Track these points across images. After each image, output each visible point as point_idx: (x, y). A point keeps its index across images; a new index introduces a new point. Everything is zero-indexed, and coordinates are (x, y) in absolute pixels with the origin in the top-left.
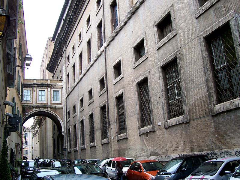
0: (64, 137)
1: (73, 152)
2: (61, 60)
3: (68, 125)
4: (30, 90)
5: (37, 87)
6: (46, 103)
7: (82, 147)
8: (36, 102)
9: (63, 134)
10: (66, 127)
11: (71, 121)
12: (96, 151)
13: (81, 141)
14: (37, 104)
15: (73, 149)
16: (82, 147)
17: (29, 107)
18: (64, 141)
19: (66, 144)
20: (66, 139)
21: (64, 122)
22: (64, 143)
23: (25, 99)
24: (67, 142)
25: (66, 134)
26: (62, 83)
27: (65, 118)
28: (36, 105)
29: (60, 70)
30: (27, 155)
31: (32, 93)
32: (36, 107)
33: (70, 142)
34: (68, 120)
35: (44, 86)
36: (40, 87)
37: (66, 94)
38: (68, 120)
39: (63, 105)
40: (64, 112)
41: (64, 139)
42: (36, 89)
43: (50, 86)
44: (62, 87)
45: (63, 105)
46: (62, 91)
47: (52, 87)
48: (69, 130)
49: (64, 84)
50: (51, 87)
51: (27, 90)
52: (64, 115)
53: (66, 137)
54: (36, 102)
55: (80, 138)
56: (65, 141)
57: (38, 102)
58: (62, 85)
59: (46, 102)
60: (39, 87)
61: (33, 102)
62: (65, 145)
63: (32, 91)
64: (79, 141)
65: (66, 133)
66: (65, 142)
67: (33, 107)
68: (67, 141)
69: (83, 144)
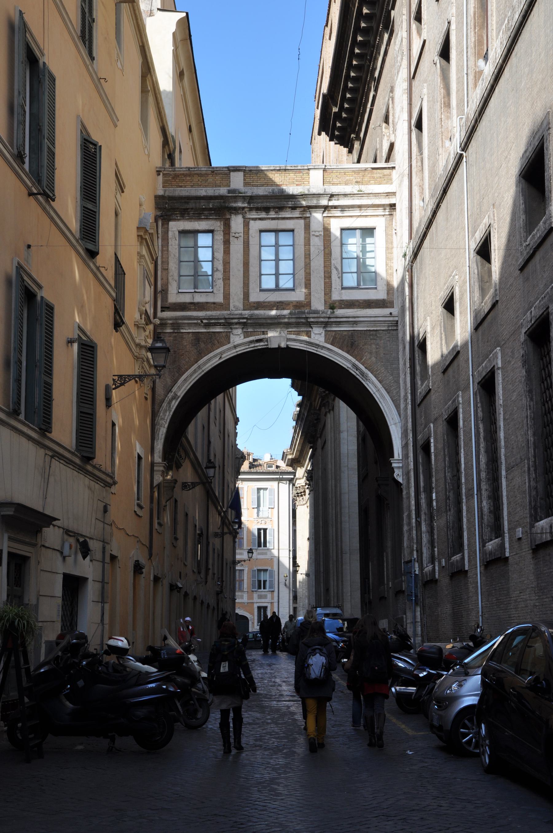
0: (404, 493)
1: (445, 582)
2: (467, 79)
3: (421, 420)
4: (292, 231)
5: (251, 209)
6: (298, 305)
7: (490, 546)
8: (246, 295)
9: (398, 475)
10: (410, 435)
11: (433, 396)
12: (224, 749)
13: (486, 510)
14: (248, 305)
15: (519, 532)
16: (490, 546)
17: (207, 325)
18: (405, 514)
19: (410, 530)
20: (413, 502)
21: (402, 406)
22: (405, 528)
23: (268, 283)
24: (419, 524)
25: (412, 474)
26: (389, 181)
27: (405, 382)
28: (247, 313)
29: (384, 111)
30: (269, 595)
31: (220, 247)
32: (244, 325)
33: (431, 518)
34: (421, 390)
35: (290, 204)
36: (267, 210)
37: (411, 238)
38: (421, 390)
39: (395, 311)
40: (401, 347)
41: (405, 505)
42: (246, 225)
43: (324, 202)
44: (393, 206)
45: (395, 311)
46: (389, 227)
47: (335, 207)
48: (426, 447)
49: (400, 185)
50: (326, 208)
51: (277, 231)
52: (401, 366)
53: (413, 494)
54: (246, 295)
55: (479, 489)
56: (409, 516)
57: (255, 297)
58: (389, 194)
59: (299, 295)
60: (258, 209)
61: (227, 296)
62: (410, 539)
63: (220, 237)
64: (474, 508)
65: (412, 466)
66: (409, 524)
67: (228, 323)
68: (418, 515)
69: (497, 529)
